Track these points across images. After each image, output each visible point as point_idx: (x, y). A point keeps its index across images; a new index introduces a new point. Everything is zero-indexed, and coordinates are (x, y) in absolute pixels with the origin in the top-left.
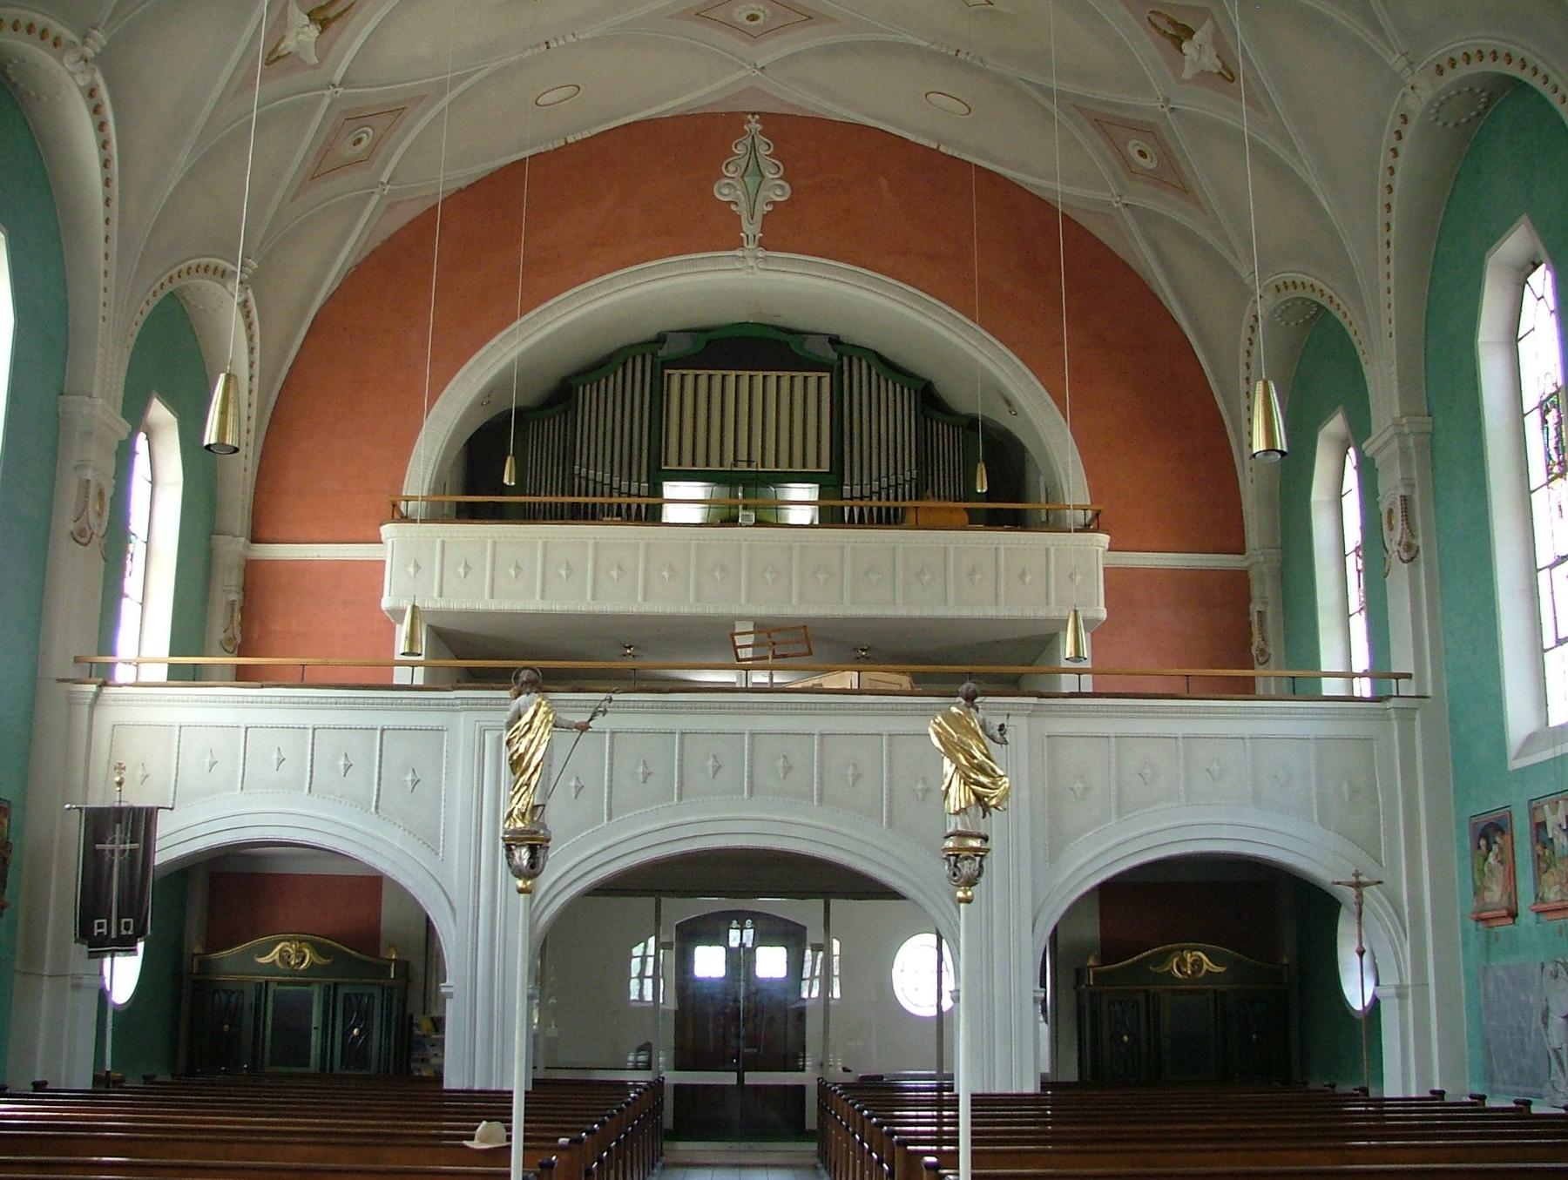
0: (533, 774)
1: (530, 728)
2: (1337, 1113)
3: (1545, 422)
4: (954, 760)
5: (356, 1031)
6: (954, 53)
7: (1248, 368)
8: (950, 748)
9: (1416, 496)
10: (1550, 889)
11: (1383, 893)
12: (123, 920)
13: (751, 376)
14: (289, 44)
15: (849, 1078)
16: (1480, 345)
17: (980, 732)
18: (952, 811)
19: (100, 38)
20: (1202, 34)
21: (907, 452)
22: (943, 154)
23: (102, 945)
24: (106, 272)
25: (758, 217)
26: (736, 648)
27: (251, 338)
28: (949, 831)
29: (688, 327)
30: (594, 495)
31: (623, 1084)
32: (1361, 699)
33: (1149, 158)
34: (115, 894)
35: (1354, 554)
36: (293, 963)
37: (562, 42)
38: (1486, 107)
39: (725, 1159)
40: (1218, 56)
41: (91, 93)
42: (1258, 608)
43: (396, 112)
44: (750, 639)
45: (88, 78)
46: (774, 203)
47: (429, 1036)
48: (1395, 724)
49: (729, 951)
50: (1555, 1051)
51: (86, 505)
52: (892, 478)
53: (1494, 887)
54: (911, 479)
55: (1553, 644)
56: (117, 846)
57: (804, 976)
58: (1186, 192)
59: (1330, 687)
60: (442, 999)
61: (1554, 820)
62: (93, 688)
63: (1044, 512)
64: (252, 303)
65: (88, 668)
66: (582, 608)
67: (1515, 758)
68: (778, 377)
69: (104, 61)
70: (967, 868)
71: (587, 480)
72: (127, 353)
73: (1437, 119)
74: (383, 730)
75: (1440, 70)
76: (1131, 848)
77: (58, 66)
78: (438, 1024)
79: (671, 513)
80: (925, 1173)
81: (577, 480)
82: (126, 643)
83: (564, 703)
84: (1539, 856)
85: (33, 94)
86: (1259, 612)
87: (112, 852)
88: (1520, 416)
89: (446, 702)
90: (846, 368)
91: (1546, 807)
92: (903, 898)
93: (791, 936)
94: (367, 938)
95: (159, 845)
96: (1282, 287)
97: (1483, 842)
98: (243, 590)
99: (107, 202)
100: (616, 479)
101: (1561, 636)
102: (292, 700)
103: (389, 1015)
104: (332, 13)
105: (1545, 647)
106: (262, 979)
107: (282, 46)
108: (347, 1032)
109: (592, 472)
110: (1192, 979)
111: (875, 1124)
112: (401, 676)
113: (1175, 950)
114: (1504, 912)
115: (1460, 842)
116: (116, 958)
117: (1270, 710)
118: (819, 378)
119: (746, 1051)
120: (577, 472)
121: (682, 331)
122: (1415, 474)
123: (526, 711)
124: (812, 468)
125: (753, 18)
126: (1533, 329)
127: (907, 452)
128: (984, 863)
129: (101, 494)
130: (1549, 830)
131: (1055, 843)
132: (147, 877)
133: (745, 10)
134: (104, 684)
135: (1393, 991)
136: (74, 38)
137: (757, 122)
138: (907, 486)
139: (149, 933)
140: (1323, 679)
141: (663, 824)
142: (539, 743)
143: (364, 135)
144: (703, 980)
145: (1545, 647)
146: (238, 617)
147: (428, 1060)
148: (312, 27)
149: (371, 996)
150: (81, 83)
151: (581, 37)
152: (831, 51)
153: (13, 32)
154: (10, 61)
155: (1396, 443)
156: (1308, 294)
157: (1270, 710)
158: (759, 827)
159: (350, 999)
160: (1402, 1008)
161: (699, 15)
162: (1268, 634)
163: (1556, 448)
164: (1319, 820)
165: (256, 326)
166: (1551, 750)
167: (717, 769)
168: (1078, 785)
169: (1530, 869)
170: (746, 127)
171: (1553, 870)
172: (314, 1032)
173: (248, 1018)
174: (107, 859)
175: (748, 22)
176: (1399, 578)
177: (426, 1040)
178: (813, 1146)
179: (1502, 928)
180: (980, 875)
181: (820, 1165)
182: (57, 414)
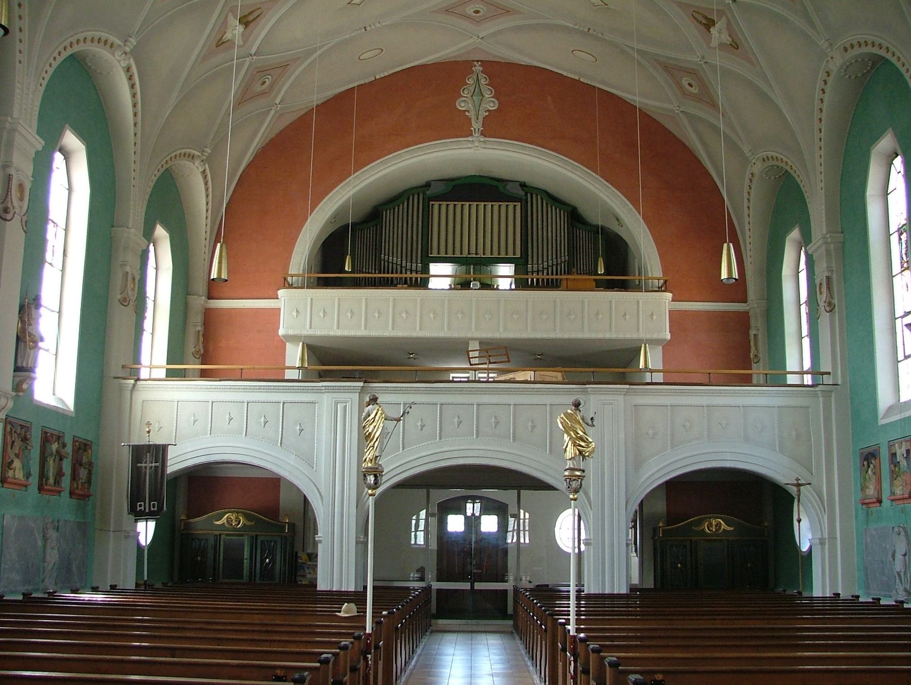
0: (375, 442)
1: (374, 421)
2: (794, 603)
3: (900, 239)
4: (569, 435)
5: (267, 560)
6: (587, 30)
7: (749, 201)
8: (567, 429)
9: (834, 277)
10: (897, 488)
11: (811, 487)
12: (152, 503)
13: (477, 205)
14: (228, 36)
15: (531, 586)
16: (867, 196)
17: (581, 421)
18: (568, 458)
19: (133, 41)
20: (720, 24)
21: (563, 246)
22: (582, 82)
23: (140, 515)
24: (135, 161)
25: (481, 119)
26: (469, 358)
27: (207, 190)
28: (567, 467)
29: (440, 178)
30: (392, 273)
31: (408, 588)
32: (808, 386)
33: (694, 87)
34: (147, 490)
35: (805, 304)
36: (234, 524)
37: (373, 27)
38: (871, 68)
39: (465, 628)
40: (730, 36)
41: (128, 69)
42: (754, 332)
43: (284, 67)
44: (476, 354)
45: (127, 62)
46: (489, 111)
47: (306, 563)
48: (821, 399)
49: (466, 518)
50: (899, 574)
51: (126, 286)
52: (555, 260)
53: (871, 487)
54: (565, 261)
55: (903, 358)
56: (148, 465)
57: (509, 530)
58: (714, 105)
59: (791, 379)
60: (315, 544)
61: (901, 451)
62: (132, 381)
63: (637, 281)
64: (208, 171)
65: (129, 371)
66: (387, 334)
67: (883, 418)
68: (492, 205)
69: (135, 54)
70: (574, 484)
71: (388, 262)
72: (146, 203)
73: (845, 74)
74: (284, 403)
75: (846, 50)
76: (692, 461)
77: (113, 58)
78: (313, 557)
79: (433, 283)
80: (559, 627)
81: (382, 262)
82: (145, 358)
83: (379, 388)
84: (892, 471)
85: (98, 71)
86: (755, 335)
87: (146, 467)
88: (888, 235)
89: (317, 388)
90: (529, 200)
91: (897, 445)
92: (558, 490)
93: (500, 510)
94: (273, 511)
95: (169, 463)
96: (766, 159)
97: (865, 463)
98: (204, 324)
99: (135, 125)
100: (404, 262)
101: (907, 354)
102: (236, 387)
103: (285, 552)
104: (251, 18)
105: (899, 360)
106: (217, 533)
107: (225, 37)
108: (263, 561)
109: (391, 258)
110: (715, 534)
111: (540, 606)
112: (290, 374)
113: (707, 518)
114: (875, 500)
115: (854, 462)
116: (149, 523)
117: (754, 392)
118: (515, 206)
119: (475, 571)
120: (382, 258)
121: (438, 180)
122: (833, 264)
123: (372, 413)
124: (511, 255)
125: (477, 12)
126: (895, 189)
127: (563, 246)
128: (583, 483)
129: (134, 279)
130: (898, 457)
131: (637, 462)
132: (164, 478)
133: (472, 8)
134: (138, 379)
135: (818, 541)
136: (120, 43)
137: (480, 66)
138: (563, 265)
139: (165, 509)
140: (788, 375)
141: (432, 452)
142: (378, 427)
143: (267, 80)
144: (452, 533)
145: (899, 360)
146: (201, 339)
147: (305, 576)
148: (241, 26)
149: (275, 542)
150: (123, 65)
151: (384, 24)
152: (519, 29)
153: (91, 44)
154: (88, 56)
155: (823, 248)
156: (779, 164)
157: (754, 392)
158: (482, 453)
159: (265, 544)
160: (823, 549)
161: (448, 11)
162: (759, 348)
163: (906, 254)
164: (779, 450)
165: (210, 183)
166: (899, 415)
167: (460, 423)
168: (650, 432)
169: (888, 477)
170: (473, 69)
171: (898, 478)
172: (245, 561)
173: (210, 555)
174: (143, 471)
175: (474, 14)
176: (824, 319)
177: (304, 565)
178: (511, 622)
179: (875, 508)
180: (580, 488)
181: (514, 631)
182: (111, 238)
